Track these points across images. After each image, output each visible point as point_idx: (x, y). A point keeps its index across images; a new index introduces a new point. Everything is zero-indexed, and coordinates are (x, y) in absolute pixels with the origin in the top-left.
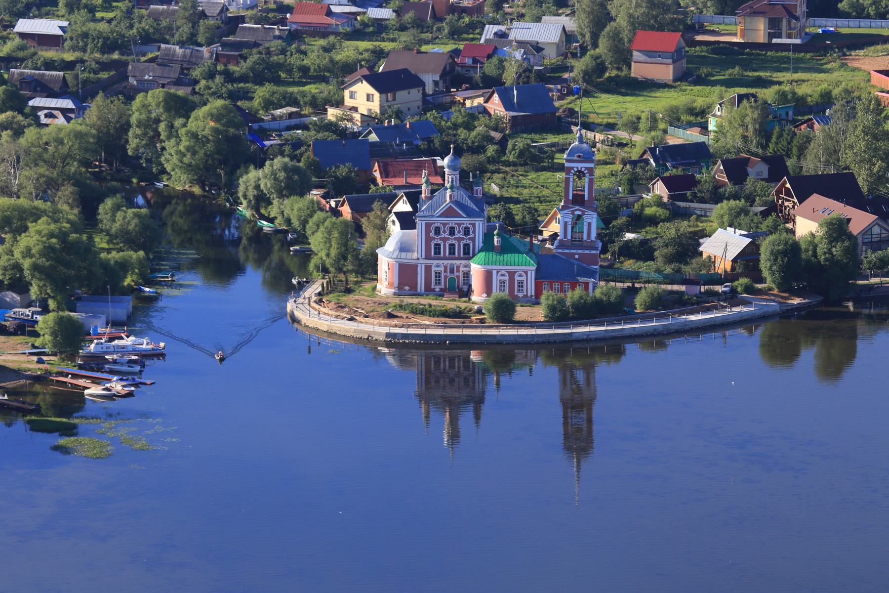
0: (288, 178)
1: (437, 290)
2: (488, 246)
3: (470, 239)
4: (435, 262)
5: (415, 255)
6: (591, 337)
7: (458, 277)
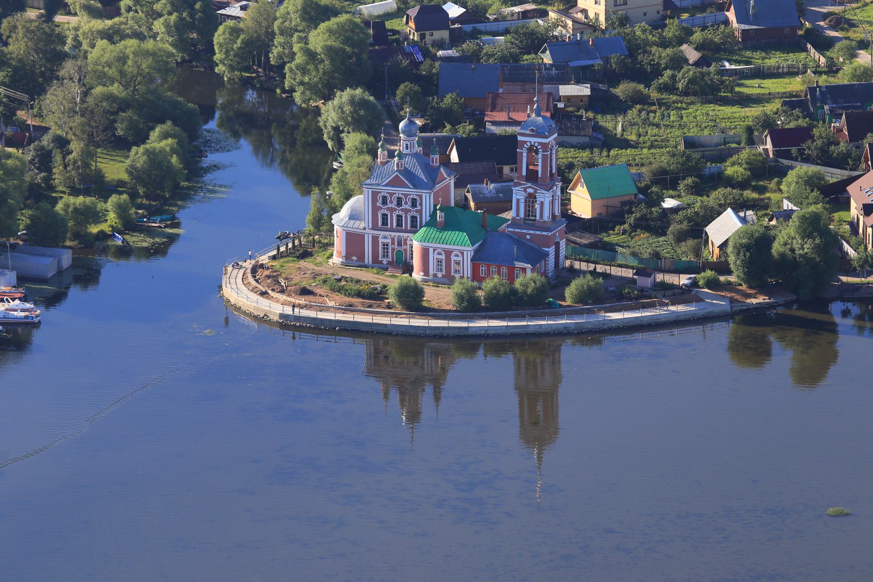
0: (354, 112)
1: (385, 262)
2: (432, 223)
3: (417, 211)
4: (382, 233)
5: (362, 225)
6: (489, 332)
7: (406, 250)
